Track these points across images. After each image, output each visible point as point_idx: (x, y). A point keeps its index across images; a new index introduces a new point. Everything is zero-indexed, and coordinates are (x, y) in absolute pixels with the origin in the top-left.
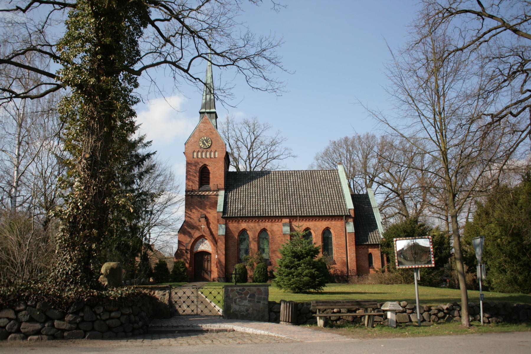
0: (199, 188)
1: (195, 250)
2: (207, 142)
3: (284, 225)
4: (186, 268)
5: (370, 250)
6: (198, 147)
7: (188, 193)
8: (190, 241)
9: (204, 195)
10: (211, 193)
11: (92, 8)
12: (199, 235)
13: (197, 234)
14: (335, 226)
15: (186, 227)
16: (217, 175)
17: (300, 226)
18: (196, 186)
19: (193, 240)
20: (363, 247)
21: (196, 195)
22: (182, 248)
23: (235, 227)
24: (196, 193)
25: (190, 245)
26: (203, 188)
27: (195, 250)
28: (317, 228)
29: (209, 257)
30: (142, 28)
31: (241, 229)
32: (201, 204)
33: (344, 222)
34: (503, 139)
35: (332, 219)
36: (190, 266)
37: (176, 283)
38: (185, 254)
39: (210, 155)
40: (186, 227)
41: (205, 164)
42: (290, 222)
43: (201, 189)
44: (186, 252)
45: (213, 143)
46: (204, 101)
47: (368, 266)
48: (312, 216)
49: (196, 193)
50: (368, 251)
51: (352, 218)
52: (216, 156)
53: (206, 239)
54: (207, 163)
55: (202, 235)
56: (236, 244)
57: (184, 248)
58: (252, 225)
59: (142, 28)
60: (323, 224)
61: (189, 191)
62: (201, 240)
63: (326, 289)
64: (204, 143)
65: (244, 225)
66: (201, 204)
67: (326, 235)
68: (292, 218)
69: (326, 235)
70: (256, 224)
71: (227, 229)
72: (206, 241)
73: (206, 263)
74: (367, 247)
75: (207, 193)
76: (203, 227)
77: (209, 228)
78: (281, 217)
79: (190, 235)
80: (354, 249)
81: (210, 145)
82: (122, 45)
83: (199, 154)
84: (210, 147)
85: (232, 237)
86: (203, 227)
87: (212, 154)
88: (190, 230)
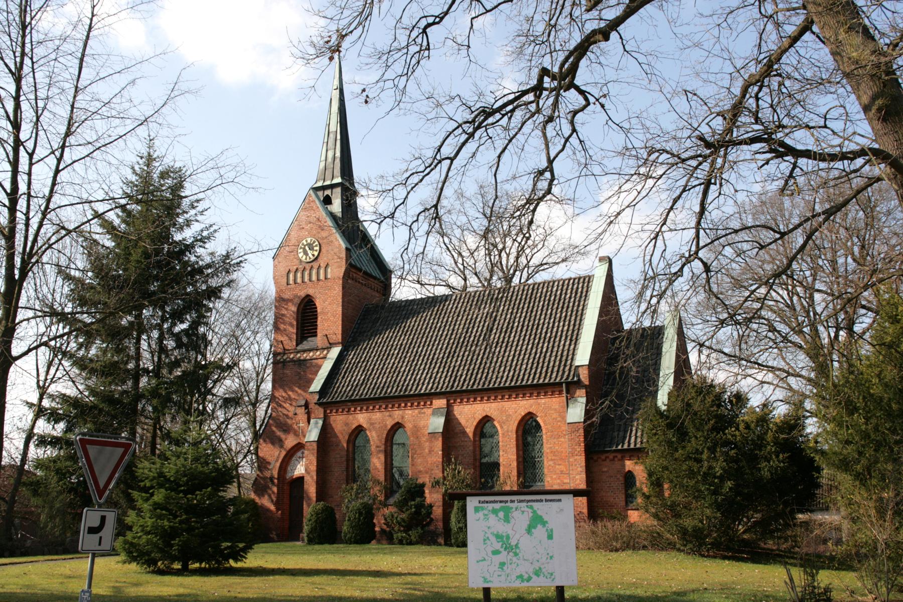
0: (297, 345)
2: (311, 249)
3: (436, 412)
5: (629, 465)
6: (297, 262)
7: (278, 358)
9: (299, 360)
10: (318, 353)
12: (295, 443)
13: (290, 441)
14: (544, 407)
15: (274, 429)
16: (329, 315)
17: (468, 414)
18: (290, 344)
19: (284, 453)
20: (611, 456)
21: (292, 360)
23: (342, 423)
24: (292, 356)
26: (305, 345)
27: (288, 476)
28: (507, 413)
31: (354, 427)
32: (300, 378)
33: (565, 398)
34: (67, 239)
35: (538, 395)
39: (318, 274)
40: (274, 429)
41: (308, 296)
42: (449, 406)
43: (299, 348)
45: (323, 250)
46: (323, 164)
47: (623, 503)
48: (494, 390)
49: (292, 356)
50: (624, 466)
51: (586, 387)
52: (329, 276)
54: (311, 292)
56: (344, 459)
58: (377, 416)
60: (518, 407)
61: (279, 354)
62: (299, 454)
63: (253, 560)
64: (306, 253)
65: (361, 418)
66: (300, 378)
67: (529, 428)
68: (454, 395)
69: (529, 428)
70: (532, 401)
71: (326, 431)
74: (619, 456)
75: (311, 354)
76: (301, 425)
78: (430, 396)
79: (277, 442)
80: (584, 464)
81: (316, 254)
83: (299, 275)
84: (316, 259)
85: (337, 445)
87: (322, 271)
88: (279, 433)
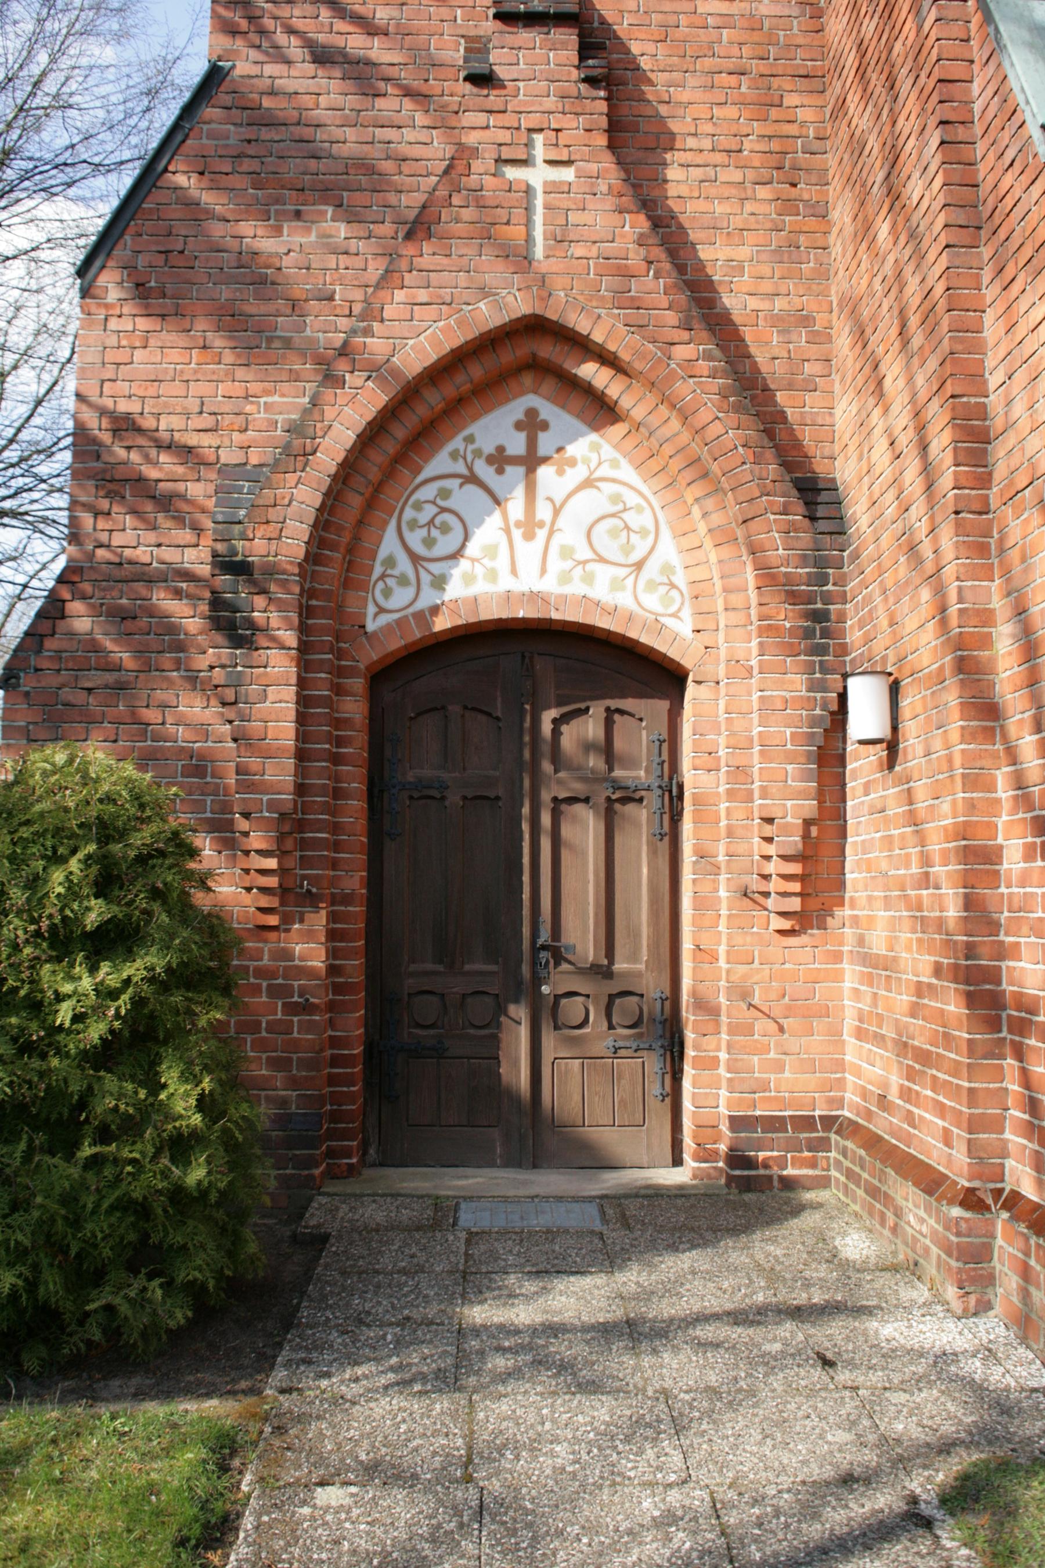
1: (392, 606)
4: (210, 964)
8: (296, 451)
11: (299, 1304)
22: (131, 539)
25: (303, 495)
29: (638, 738)
30: (192, 865)
36: (292, 897)
37: (526, 931)
38: (211, 655)
44: (234, 628)
53: (601, 411)
55: (535, 326)
57: (197, 559)
59: (192, 865)
62: (496, 428)
72: (590, 450)
73: (585, 829)
77: (644, 193)
82: (209, 1022)
86: (537, 176)
